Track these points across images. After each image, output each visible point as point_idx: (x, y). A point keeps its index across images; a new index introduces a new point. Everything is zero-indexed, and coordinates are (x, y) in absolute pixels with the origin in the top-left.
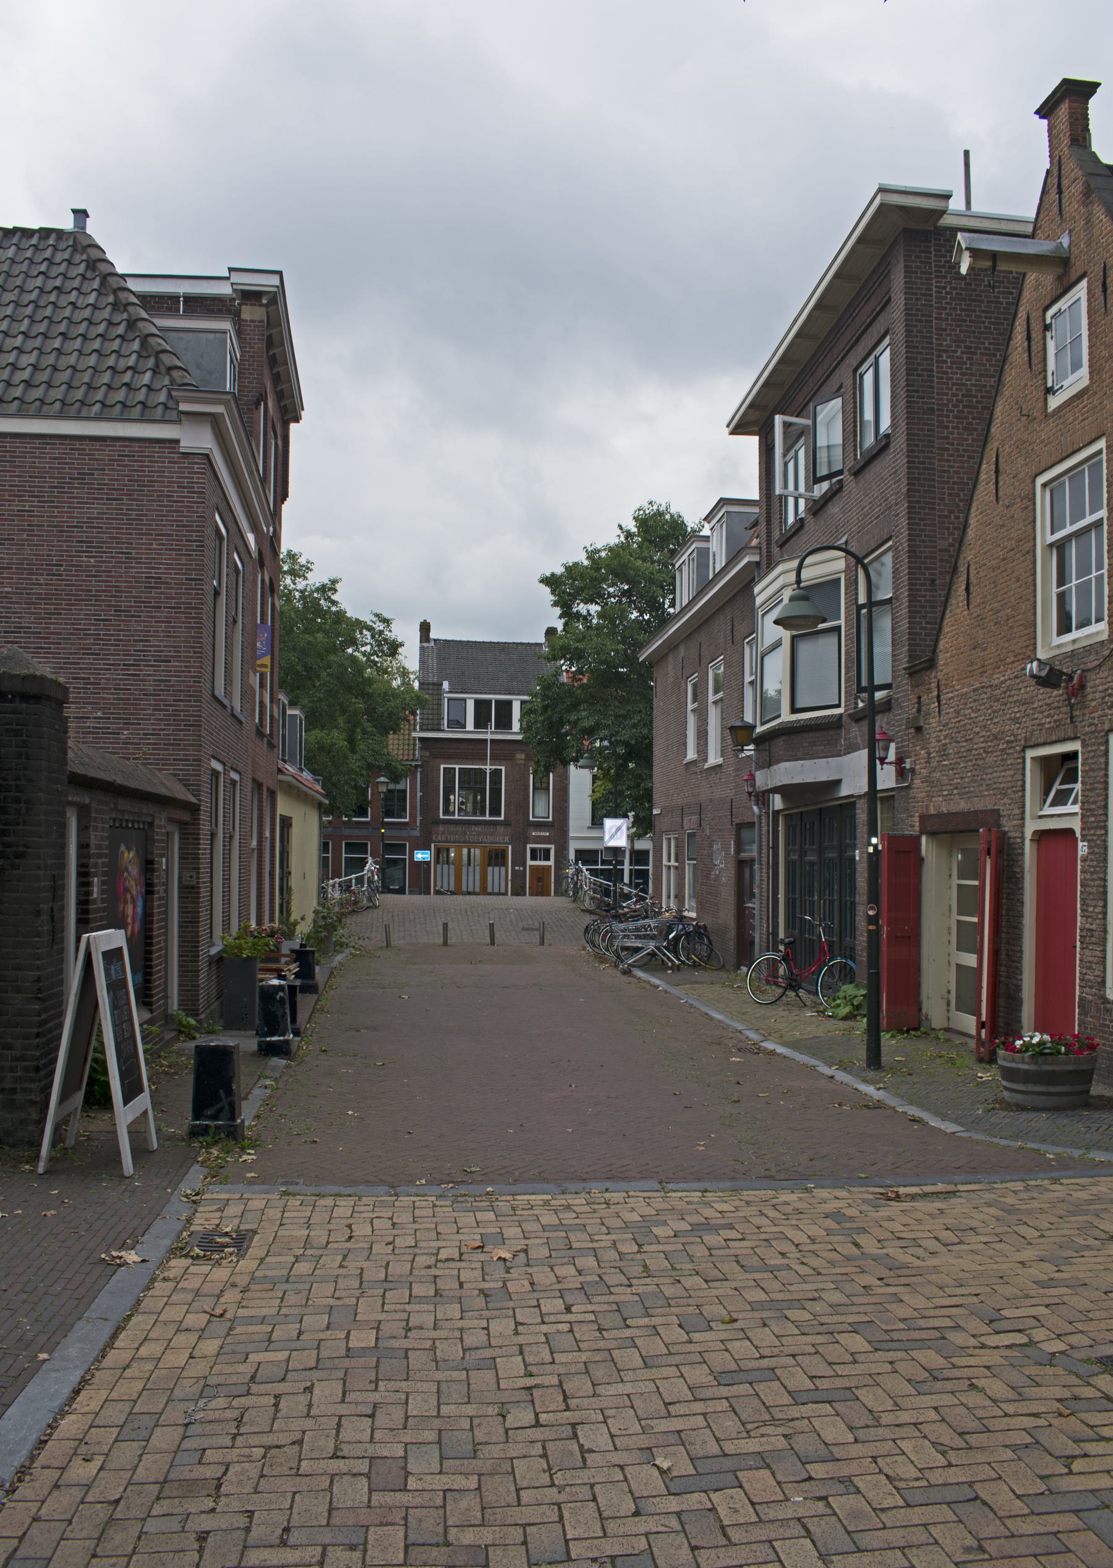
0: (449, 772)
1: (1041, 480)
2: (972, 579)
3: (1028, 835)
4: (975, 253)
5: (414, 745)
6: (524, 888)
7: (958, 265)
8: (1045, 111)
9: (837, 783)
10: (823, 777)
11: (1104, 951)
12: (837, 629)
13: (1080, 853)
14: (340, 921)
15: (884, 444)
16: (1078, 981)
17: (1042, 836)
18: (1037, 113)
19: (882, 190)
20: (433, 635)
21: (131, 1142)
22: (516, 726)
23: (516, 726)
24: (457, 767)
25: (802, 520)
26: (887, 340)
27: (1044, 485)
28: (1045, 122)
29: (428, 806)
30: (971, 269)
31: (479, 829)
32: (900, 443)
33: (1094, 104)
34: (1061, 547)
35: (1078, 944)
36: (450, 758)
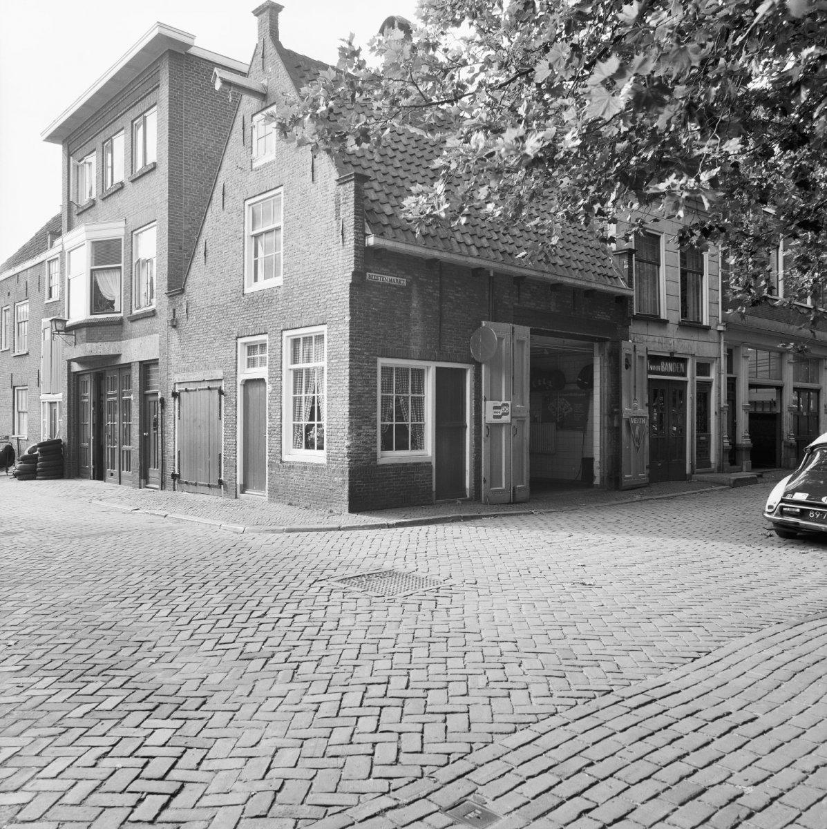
1: (248, 202)
2: (208, 248)
3: (239, 382)
4: (225, 82)
7: (213, 85)
8: (258, 12)
9: (118, 356)
10: (111, 353)
11: (281, 437)
12: (120, 268)
13: (267, 390)
14: (737, 251)
15: (154, 167)
16: (267, 454)
17: (248, 383)
18: (253, 12)
19: (160, 25)
21: (659, 247)
22: (504, 484)
23: (504, 484)
25: (94, 201)
27: (249, 205)
30: (221, 89)
32: (164, 169)
33: (280, 14)
34: (257, 237)
35: (267, 435)
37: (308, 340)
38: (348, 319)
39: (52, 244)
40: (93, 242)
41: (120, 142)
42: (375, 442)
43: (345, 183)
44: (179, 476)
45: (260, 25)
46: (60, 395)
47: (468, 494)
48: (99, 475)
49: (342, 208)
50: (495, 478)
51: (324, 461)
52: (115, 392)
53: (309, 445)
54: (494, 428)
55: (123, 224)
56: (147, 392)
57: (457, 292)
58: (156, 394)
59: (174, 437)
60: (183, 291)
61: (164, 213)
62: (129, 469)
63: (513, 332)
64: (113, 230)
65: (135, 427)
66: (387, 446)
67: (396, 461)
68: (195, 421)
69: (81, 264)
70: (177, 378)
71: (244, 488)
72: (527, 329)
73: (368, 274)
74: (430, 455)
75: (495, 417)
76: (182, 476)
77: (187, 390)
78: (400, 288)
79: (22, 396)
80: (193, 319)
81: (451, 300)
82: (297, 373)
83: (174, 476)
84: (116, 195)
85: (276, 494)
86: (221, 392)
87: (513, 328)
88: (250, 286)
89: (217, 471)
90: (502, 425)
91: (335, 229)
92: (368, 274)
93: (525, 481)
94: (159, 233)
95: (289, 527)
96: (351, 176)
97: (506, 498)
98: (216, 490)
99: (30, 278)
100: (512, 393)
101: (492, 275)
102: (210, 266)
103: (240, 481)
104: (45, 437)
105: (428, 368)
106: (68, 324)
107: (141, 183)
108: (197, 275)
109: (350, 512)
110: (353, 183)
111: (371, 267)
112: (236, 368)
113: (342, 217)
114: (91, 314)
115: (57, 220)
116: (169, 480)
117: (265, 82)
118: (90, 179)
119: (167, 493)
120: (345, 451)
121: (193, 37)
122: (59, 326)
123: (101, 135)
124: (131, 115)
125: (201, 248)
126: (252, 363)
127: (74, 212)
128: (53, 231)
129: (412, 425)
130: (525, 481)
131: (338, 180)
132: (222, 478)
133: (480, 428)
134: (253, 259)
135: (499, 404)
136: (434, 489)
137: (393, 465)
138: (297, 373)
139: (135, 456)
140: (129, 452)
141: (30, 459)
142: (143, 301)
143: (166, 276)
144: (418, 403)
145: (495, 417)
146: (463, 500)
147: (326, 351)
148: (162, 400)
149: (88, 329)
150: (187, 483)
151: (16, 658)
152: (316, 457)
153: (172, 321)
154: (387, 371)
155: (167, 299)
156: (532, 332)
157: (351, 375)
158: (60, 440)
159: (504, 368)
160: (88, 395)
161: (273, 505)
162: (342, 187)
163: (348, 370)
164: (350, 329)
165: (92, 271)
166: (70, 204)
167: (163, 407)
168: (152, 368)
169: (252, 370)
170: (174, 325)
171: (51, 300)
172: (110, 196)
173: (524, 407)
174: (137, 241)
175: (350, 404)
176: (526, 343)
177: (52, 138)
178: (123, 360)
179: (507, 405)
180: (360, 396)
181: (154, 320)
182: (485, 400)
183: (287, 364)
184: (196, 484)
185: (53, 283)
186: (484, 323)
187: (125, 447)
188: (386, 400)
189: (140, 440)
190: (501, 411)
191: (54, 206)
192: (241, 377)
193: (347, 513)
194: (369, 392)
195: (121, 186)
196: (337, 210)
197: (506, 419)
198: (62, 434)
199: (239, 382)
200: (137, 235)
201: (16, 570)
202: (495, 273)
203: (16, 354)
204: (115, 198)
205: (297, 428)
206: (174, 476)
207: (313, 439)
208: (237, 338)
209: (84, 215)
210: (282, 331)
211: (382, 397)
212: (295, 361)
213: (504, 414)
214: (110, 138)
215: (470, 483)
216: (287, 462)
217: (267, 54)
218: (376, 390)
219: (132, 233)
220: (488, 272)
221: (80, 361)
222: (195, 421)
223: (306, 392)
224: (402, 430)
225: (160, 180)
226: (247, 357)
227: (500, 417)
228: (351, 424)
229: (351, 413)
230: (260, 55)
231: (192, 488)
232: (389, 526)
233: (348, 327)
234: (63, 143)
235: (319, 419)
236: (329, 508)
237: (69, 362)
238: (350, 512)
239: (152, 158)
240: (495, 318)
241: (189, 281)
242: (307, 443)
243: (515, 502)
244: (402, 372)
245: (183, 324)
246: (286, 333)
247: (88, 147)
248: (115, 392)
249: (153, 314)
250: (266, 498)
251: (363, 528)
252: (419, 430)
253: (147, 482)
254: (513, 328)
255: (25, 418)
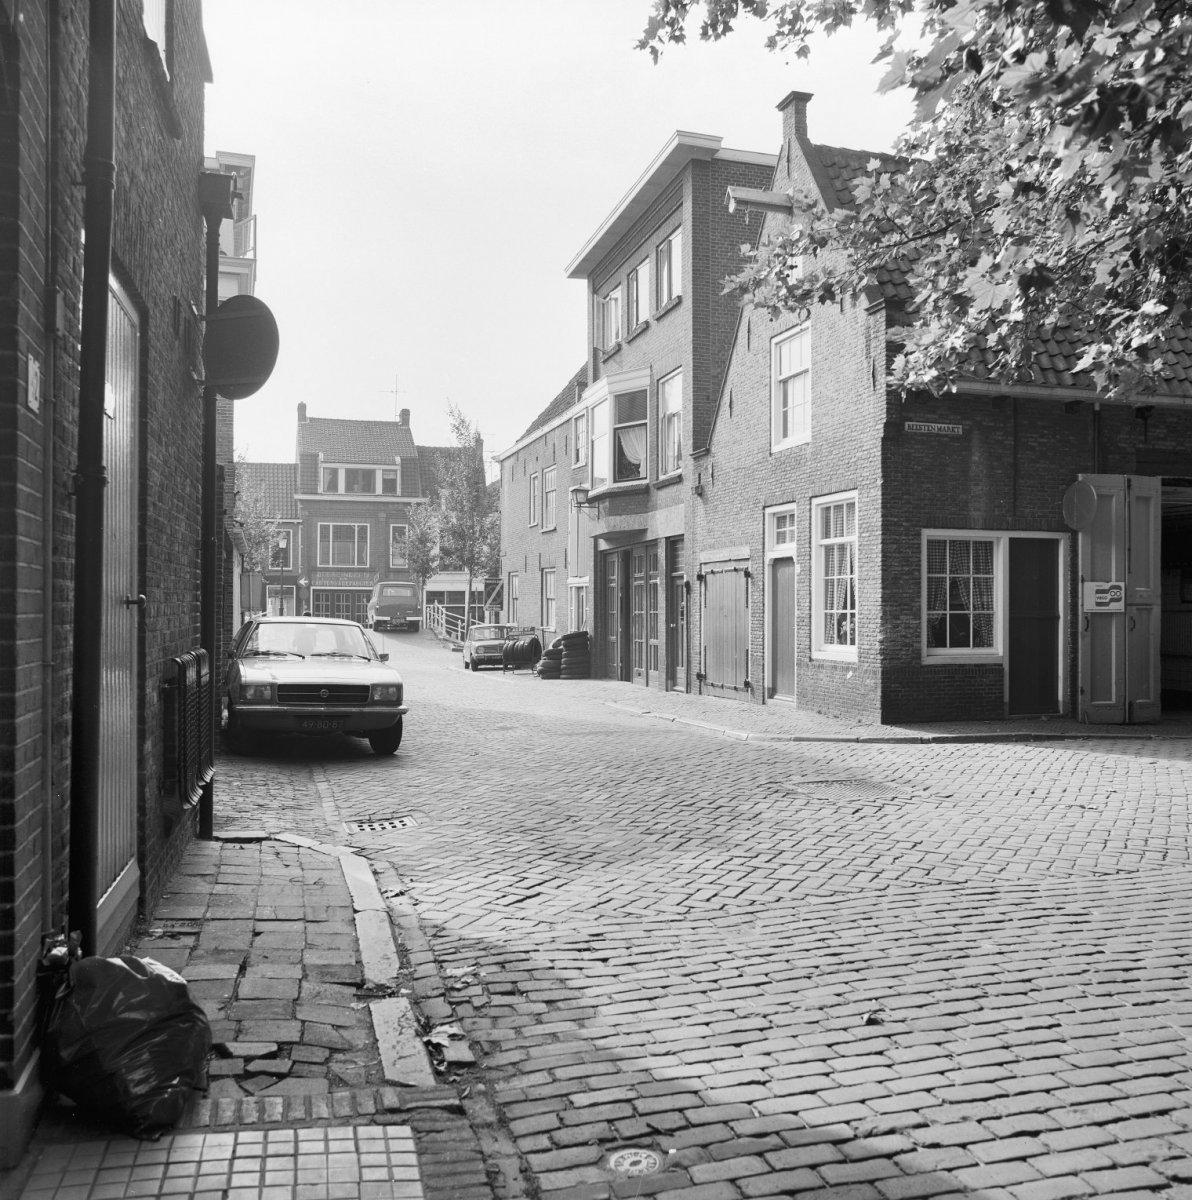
0: (325, 529)
1: (775, 341)
3: (767, 562)
4: (739, 202)
5: (296, 506)
6: (976, 550)
7: (727, 208)
8: (782, 106)
10: (636, 527)
12: (645, 424)
17: (778, 562)
18: (778, 107)
19: (680, 133)
20: (309, 414)
22: (1114, 697)
23: (1114, 697)
24: (331, 524)
26: (680, 229)
28: (781, 113)
29: (309, 557)
30: (736, 210)
31: (350, 575)
32: (688, 303)
33: (809, 105)
36: (325, 517)
37: (839, 507)
38: (880, 482)
39: (580, 397)
40: (616, 396)
41: (645, 272)
42: (919, 636)
43: (875, 313)
44: (705, 677)
45: (785, 120)
46: (587, 579)
47: (1061, 708)
48: (627, 676)
49: (873, 345)
50: (1099, 688)
51: (855, 659)
52: (642, 574)
53: (842, 639)
54: (1093, 619)
55: (648, 372)
56: (674, 574)
57: (1042, 437)
58: (682, 577)
59: (702, 627)
60: (708, 452)
61: (689, 358)
62: (656, 668)
63: (1129, 486)
64: (639, 381)
65: (662, 618)
66: (937, 640)
67: (949, 661)
68: (721, 609)
69: (604, 420)
70: (703, 557)
71: (773, 692)
72: (1156, 481)
73: (907, 424)
74: (1001, 654)
75: (1098, 604)
76: (708, 677)
77: (712, 572)
78: (955, 438)
79: (551, 579)
80: (719, 484)
81: (1032, 449)
82: (829, 549)
83: (700, 676)
84: (643, 337)
85: (805, 699)
86: (747, 574)
87: (1129, 481)
88: (778, 443)
89: (744, 671)
90: (1111, 615)
91: (865, 371)
92: (907, 424)
93: (1152, 695)
94: (684, 381)
95: (798, 735)
96: (880, 304)
97: (1118, 717)
98: (743, 694)
99: (557, 439)
100: (1129, 570)
101: (1097, 408)
102: (735, 419)
103: (768, 683)
104: (572, 629)
105: (998, 539)
106: (591, 494)
107: (666, 321)
108: (724, 430)
109: (883, 723)
110: (884, 313)
111: (911, 415)
112: (764, 544)
113: (872, 354)
114: (615, 481)
115: (584, 371)
116: (695, 682)
117: (790, 192)
118: (616, 317)
119: (692, 697)
120: (878, 646)
121: (719, 140)
122: (581, 497)
123: (626, 265)
124: (655, 239)
125: (726, 399)
126: (781, 538)
127: (601, 358)
128: (580, 383)
129: (974, 616)
130: (1152, 695)
131: (867, 310)
132: (749, 679)
133: (1077, 619)
134: (782, 410)
135: (1106, 586)
136: (1007, 698)
137: (944, 666)
138: (829, 549)
139: (662, 652)
140: (656, 647)
141: (554, 654)
142: (670, 467)
143: (691, 434)
144: (984, 589)
145: (1098, 604)
146: (1052, 717)
147: (856, 521)
148: (688, 584)
149: (614, 501)
150: (712, 685)
151: (465, 817)
152: (847, 653)
153: (697, 488)
154: (933, 544)
155: (692, 461)
156: (1164, 483)
157: (883, 551)
158: (586, 633)
159: (1114, 537)
160: (615, 580)
161: (802, 713)
162: (872, 317)
163: (880, 546)
164: (883, 494)
165: (616, 430)
166: (595, 351)
167: (688, 592)
168: (679, 546)
169: (782, 546)
170: (700, 491)
171: (578, 465)
172: (634, 338)
173: (1151, 588)
174: (663, 388)
175: (883, 588)
176: (1152, 502)
177: (575, 274)
178: (650, 537)
179: (1119, 588)
180: (896, 579)
181: (679, 487)
182: (1083, 581)
183: (818, 540)
184: (722, 687)
185: (580, 446)
186: (1080, 477)
187: (653, 641)
188: (935, 585)
189: (667, 632)
190: (1109, 596)
191: (581, 357)
192: (770, 555)
193: (879, 723)
194: (909, 573)
195: (647, 325)
196: (868, 346)
197: (1119, 606)
198: (589, 628)
199: (767, 562)
200: (663, 383)
201: (495, 757)
202: (1101, 405)
203: (545, 530)
204: (640, 341)
205: (829, 617)
206: (700, 676)
207: (846, 633)
208: (764, 508)
209: (611, 362)
210: (811, 498)
211: (929, 578)
212: (827, 535)
213: (1112, 600)
214: (635, 270)
215: (1064, 696)
216: (817, 660)
217: (793, 156)
218: (919, 571)
219: (658, 383)
220: (1093, 404)
221: (607, 537)
222: (721, 609)
223: (840, 574)
224: (960, 622)
225: (684, 317)
226: (776, 530)
227: (1107, 604)
228: (884, 613)
229: (885, 599)
230: (785, 159)
231: (718, 691)
232: (922, 741)
233: (880, 493)
234: (589, 277)
235: (853, 607)
236: (859, 717)
237: (596, 538)
238: (883, 723)
239: (677, 291)
240: (1104, 469)
241: (715, 439)
242: (839, 636)
243: (1131, 723)
244: (960, 547)
245: (709, 491)
246: (815, 501)
247: (613, 282)
248: (642, 574)
249: (679, 479)
250: (795, 705)
251: (888, 741)
252: (989, 620)
253: (675, 685)
254: (1129, 481)
255: (553, 605)
